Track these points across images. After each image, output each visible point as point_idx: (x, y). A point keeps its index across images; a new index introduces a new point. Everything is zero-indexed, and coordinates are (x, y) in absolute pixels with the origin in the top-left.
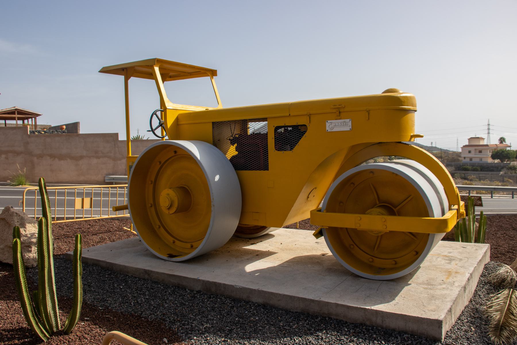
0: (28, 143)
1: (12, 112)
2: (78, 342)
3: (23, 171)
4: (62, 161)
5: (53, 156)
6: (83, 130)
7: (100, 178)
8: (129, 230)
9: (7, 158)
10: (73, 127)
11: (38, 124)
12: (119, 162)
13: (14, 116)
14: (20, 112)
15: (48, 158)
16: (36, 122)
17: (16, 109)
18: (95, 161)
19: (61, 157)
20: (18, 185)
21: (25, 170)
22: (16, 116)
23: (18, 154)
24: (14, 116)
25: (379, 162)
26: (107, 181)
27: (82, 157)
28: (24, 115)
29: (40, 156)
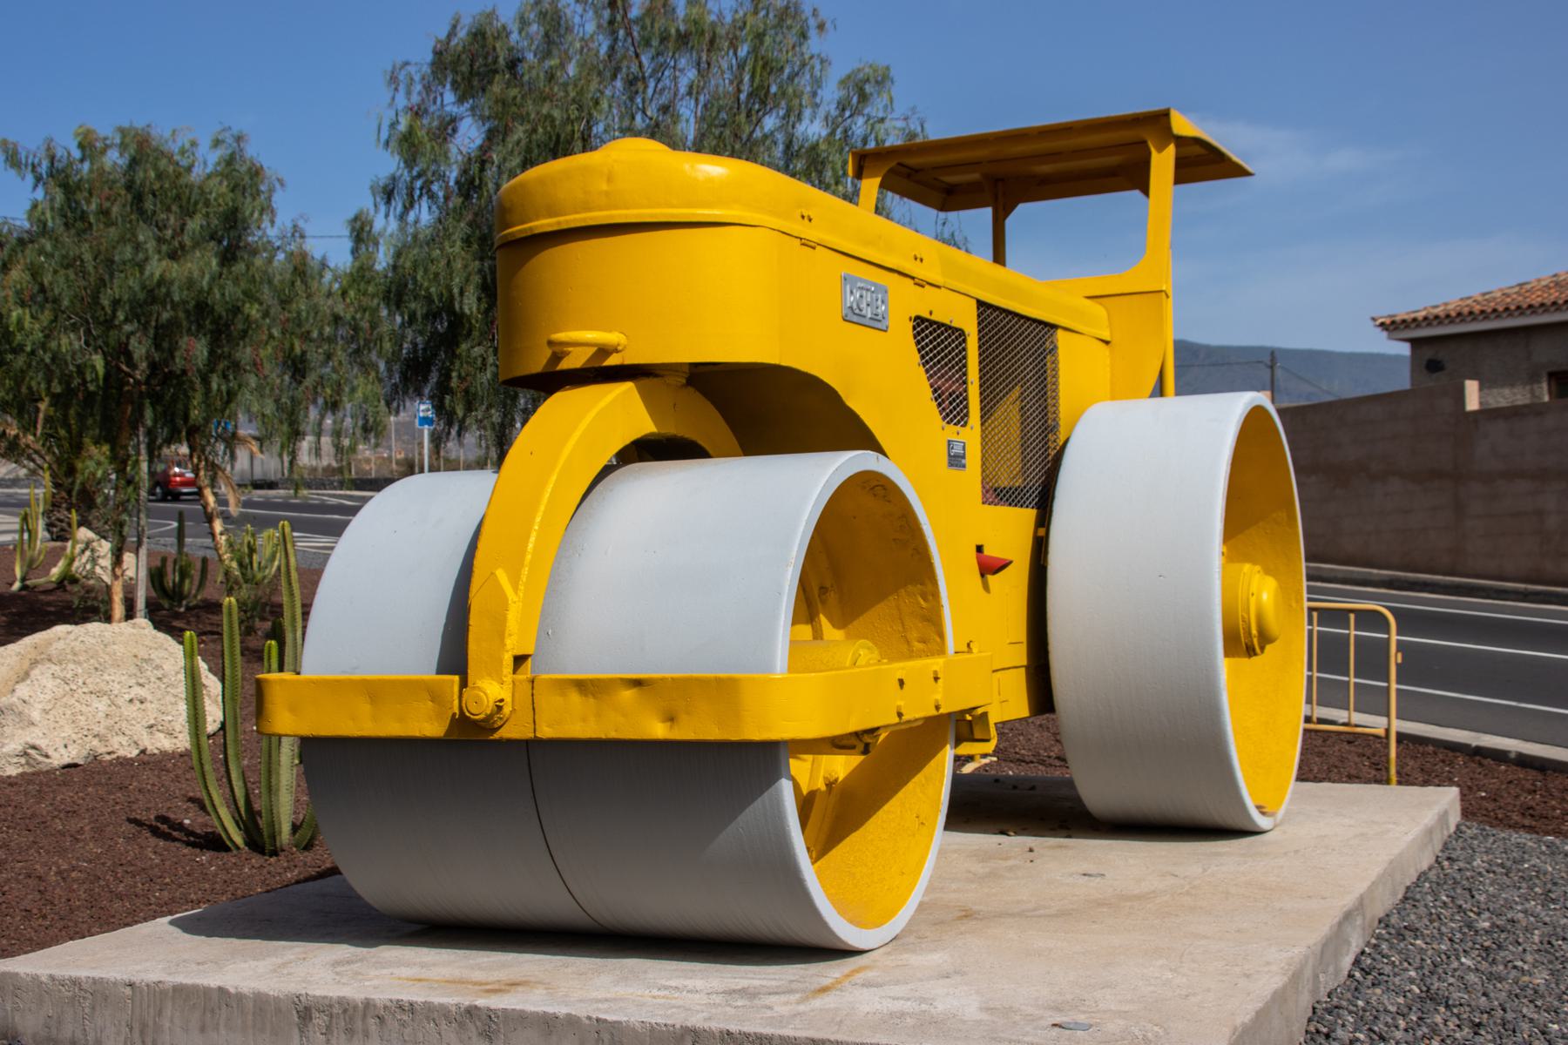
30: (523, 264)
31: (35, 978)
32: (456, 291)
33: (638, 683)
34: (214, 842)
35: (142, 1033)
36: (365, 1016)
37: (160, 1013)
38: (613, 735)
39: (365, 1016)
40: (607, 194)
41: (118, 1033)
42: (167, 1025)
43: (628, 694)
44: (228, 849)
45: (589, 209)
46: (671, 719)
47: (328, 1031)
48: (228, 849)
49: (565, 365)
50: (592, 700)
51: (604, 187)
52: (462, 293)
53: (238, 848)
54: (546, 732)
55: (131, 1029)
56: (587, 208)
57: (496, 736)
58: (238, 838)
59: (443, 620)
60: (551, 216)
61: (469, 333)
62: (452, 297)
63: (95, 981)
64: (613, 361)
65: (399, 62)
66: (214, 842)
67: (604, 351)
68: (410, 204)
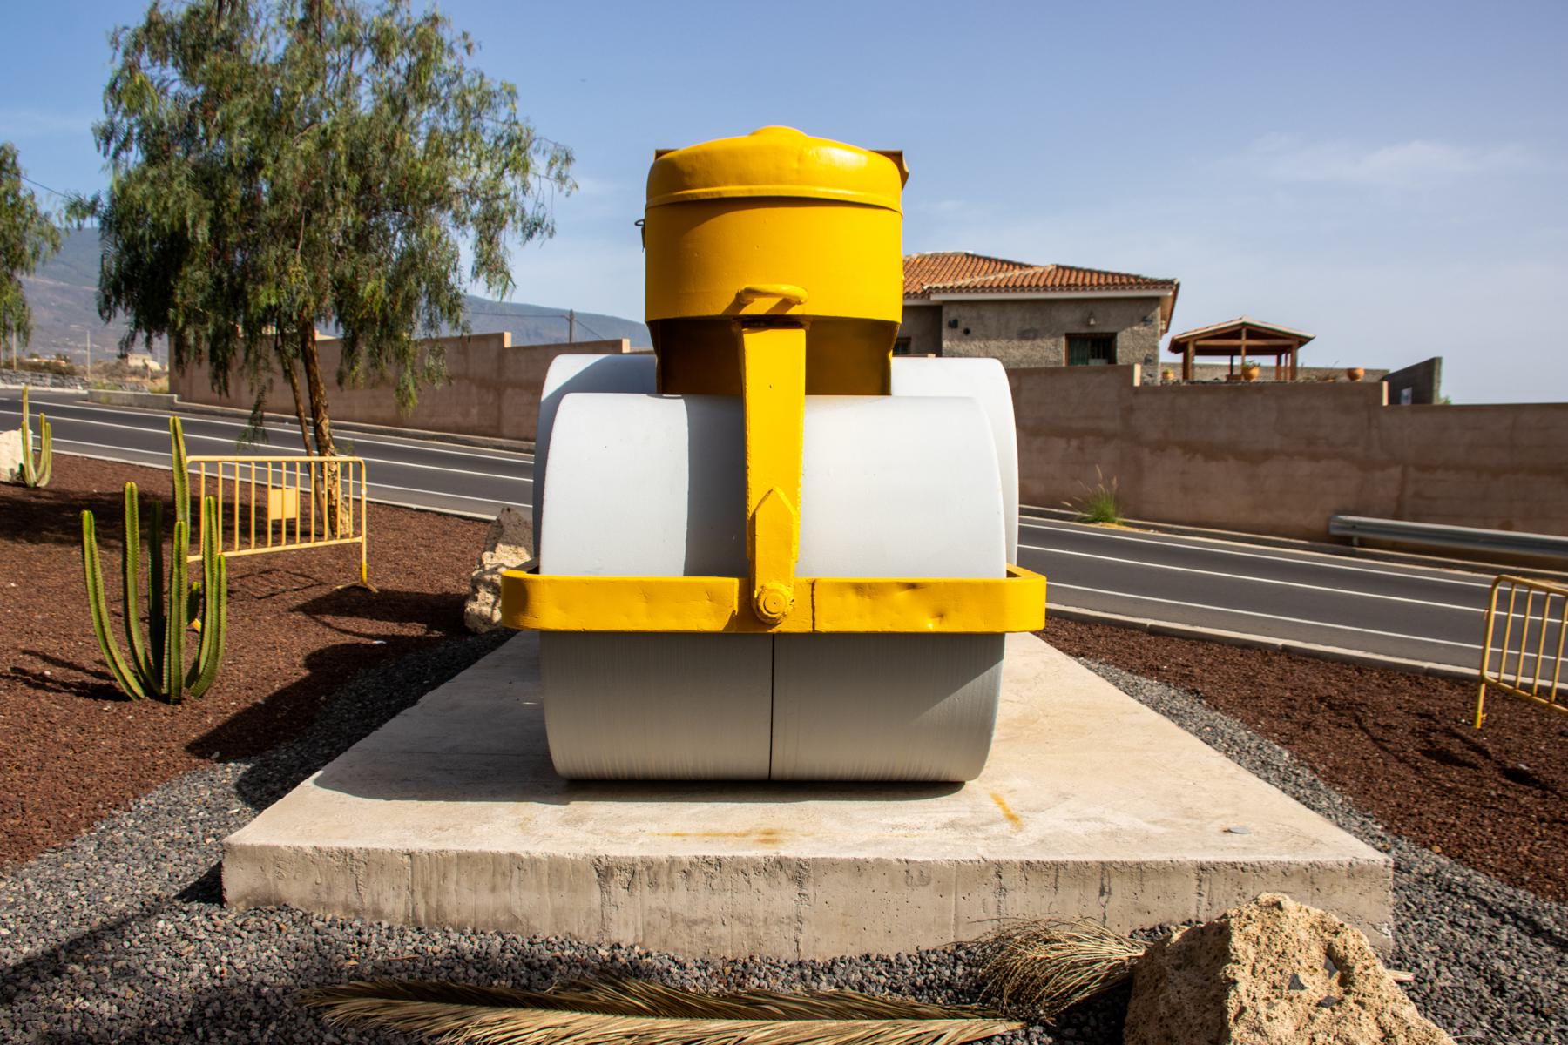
0: (1131, 410)
1: (1233, 332)
2: (402, 1041)
3: (1109, 486)
4: (1214, 463)
5: (1189, 449)
6: (1451, 390)
7: (1314, 520)
8: (1476, 672)
9: (1081, 449)
10: (1421, 378)
11: (1299, 365)
12: (1378, 475)
13: (1236, 342)
14: (1254, 332)
15: (1178, 452)
16: (1294, 361)
17: (1244, 325)
18: (1304, 468)
19: (1212, 453)
20: (1093, 521)
21: (1114, 482)
22: (1244, 342)
23: (1105, 437)
24: (1236, 342)
25: (792, 183)
26: (1335, 532)
27: (1267, 455)
28: (1283, 343)
29: (1159, 447)
30: (705, 220)
31: (297, 850)
32: (189, 223)
33: (912, 586)
34: (105, 690)
35: (425, 895)
36: (670, 871)
37: (444, 878)
38: (888, 628)
39: (670, 871)
40: (798, 172)
41: (399, 896)
42: (452, 887)
43: (902, 596)
44: (128, 699)
45: (781, 182)
46: (941, 616)
47: (629, 886)
48: (128, 699)
49: (748, 310)
50: (867, 600)
51: (796, 166)
52: (194, 225)
53: (139, 698)
54: (824, 626)
55: (412, 892)
56: (779, 181)
57: (775, 630)
58: (139, 690)
59: (685, 529)
60: (741, 183)
61: (192, 261)
62: (184, 226)
63: (368, 852)
64: (794, 311)
65: (120, 27)
66: (105, 690)
67: (787, 302)
68: (125, 146)
